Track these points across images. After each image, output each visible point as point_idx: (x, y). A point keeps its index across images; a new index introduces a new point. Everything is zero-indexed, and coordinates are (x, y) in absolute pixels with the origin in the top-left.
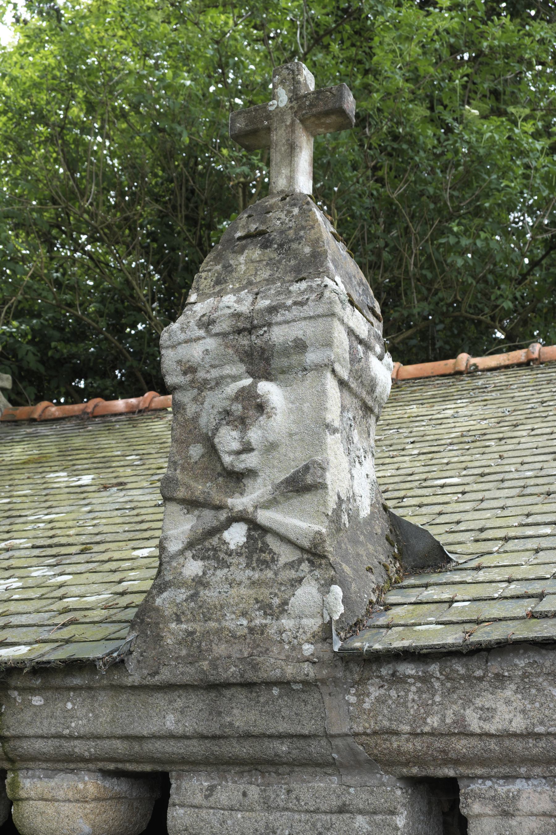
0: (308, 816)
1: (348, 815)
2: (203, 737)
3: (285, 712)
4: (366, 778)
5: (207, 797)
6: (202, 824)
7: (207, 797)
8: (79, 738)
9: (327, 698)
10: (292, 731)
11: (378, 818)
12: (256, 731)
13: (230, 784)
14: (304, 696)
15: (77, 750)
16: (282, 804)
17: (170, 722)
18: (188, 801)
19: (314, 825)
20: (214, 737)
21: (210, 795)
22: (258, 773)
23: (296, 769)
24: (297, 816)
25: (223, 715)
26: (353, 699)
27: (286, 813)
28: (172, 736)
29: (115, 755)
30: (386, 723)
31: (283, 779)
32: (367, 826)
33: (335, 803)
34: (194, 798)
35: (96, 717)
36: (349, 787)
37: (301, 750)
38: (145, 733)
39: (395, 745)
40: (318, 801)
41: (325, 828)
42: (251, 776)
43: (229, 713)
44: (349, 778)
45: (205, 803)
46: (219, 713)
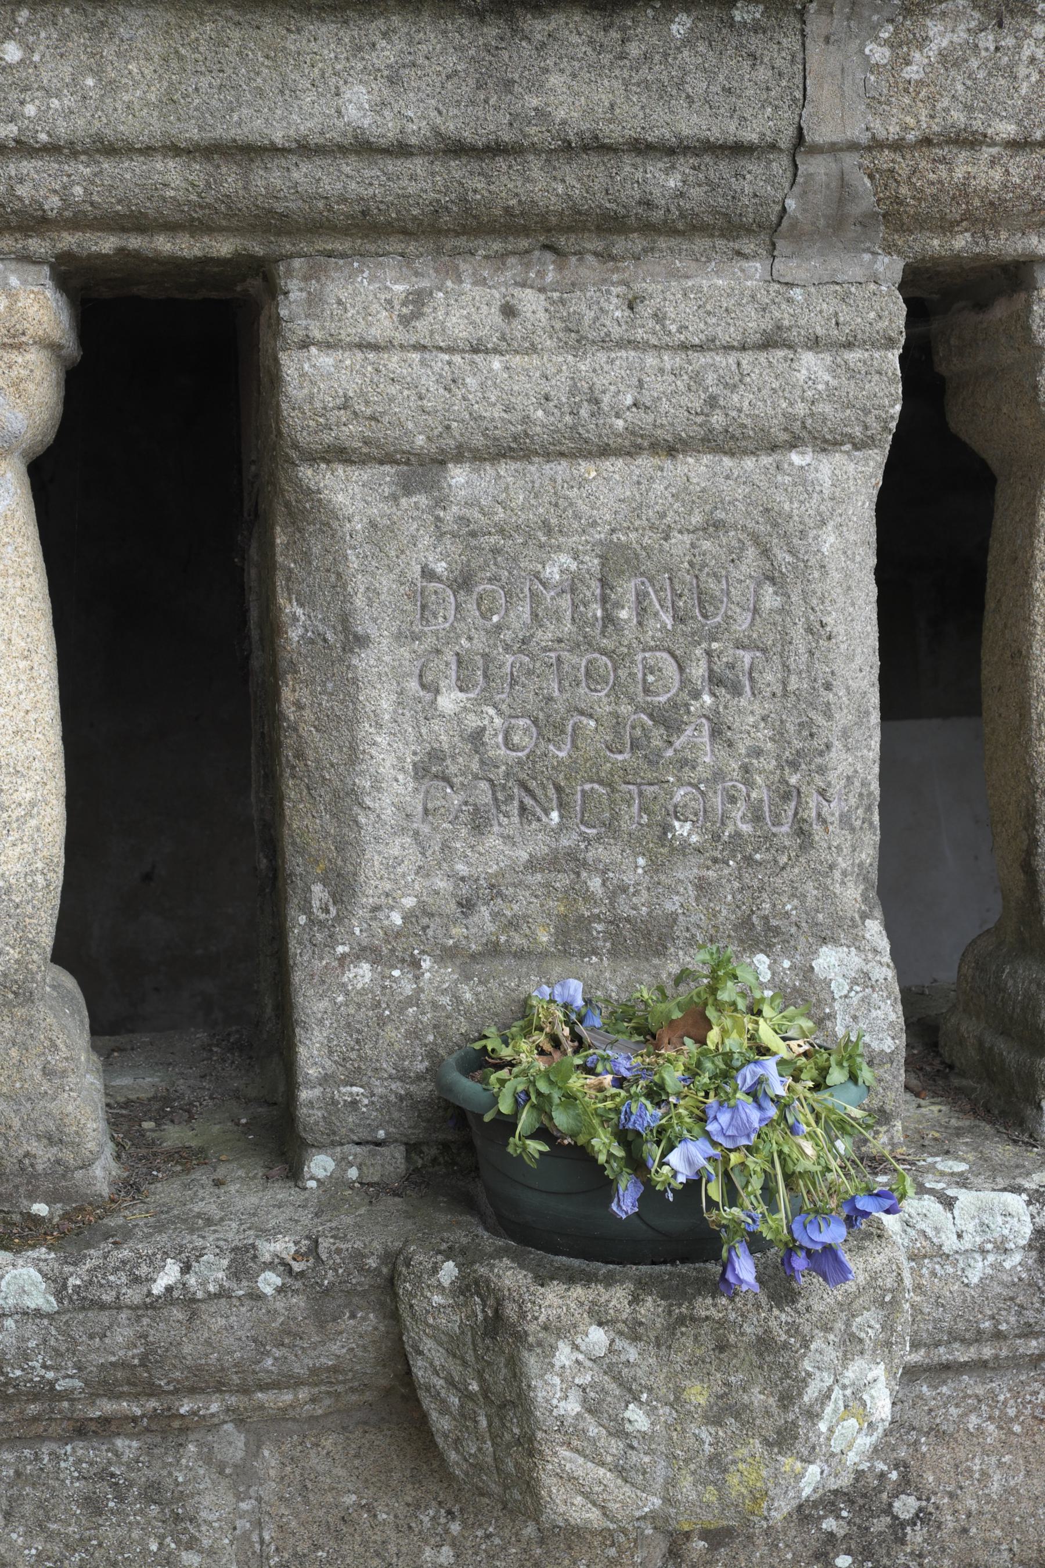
0: (679, 360)
1: (780, 353)
2: (457, 149)
3: (697, 85)
4: (836, 264)
5: (405, 321)
6: (393, 390)
7: (405, 321)
8: (52, 149)
9: (815, 49)
10: (715, 134)
11: (853, 356)
12: (613, 133)
13: (467, 286)
14: (755, 42)
15: (21, 191)
16: (616, 332)
17: (358, 107)
18: (349, 333)
19: (697, 378)
20: (496, 150)
21: (417, 315)
22: (549, 256)
23: (662, 243)
24: (651, 360)
25: (517, 89)
26: (879, 54)
27: (623, 353)
28: (364, 148)
29: (150, 208)
30: (958, 117)
31: (617, 269)
32: (827, 377)
33: (754, 323)
34: (370, 325)
35: (111, 87)
36: (790, 285)
37: (713, 187)
38: (278, 137)
39: (959, 174)
40: (712, 320)
41: (726, 385)
42: (528, 266)
43: (536, 86)
44: (793, 263)
45: (400, 336)
46: (508, 85)
